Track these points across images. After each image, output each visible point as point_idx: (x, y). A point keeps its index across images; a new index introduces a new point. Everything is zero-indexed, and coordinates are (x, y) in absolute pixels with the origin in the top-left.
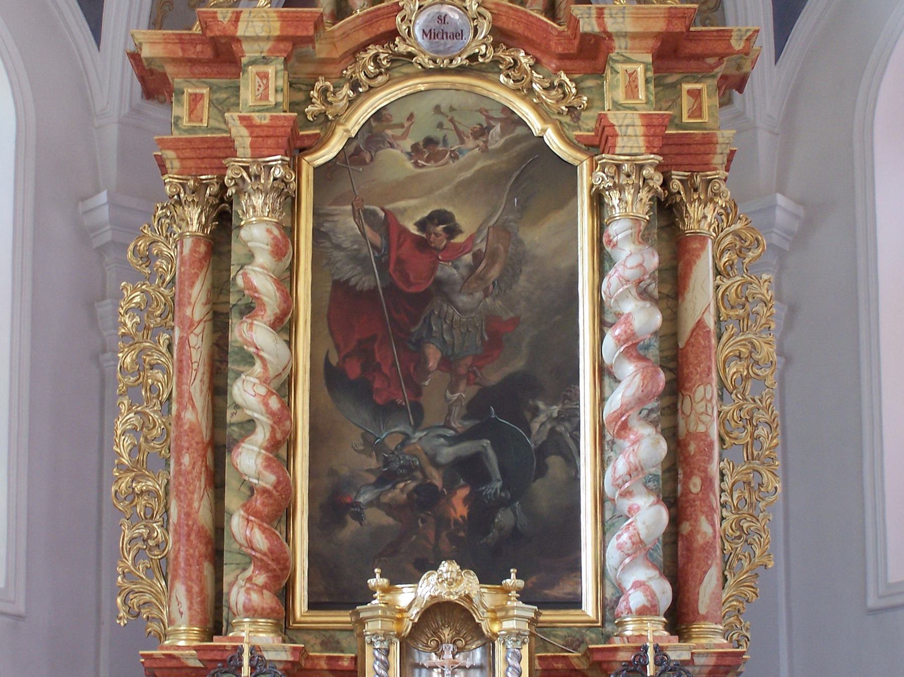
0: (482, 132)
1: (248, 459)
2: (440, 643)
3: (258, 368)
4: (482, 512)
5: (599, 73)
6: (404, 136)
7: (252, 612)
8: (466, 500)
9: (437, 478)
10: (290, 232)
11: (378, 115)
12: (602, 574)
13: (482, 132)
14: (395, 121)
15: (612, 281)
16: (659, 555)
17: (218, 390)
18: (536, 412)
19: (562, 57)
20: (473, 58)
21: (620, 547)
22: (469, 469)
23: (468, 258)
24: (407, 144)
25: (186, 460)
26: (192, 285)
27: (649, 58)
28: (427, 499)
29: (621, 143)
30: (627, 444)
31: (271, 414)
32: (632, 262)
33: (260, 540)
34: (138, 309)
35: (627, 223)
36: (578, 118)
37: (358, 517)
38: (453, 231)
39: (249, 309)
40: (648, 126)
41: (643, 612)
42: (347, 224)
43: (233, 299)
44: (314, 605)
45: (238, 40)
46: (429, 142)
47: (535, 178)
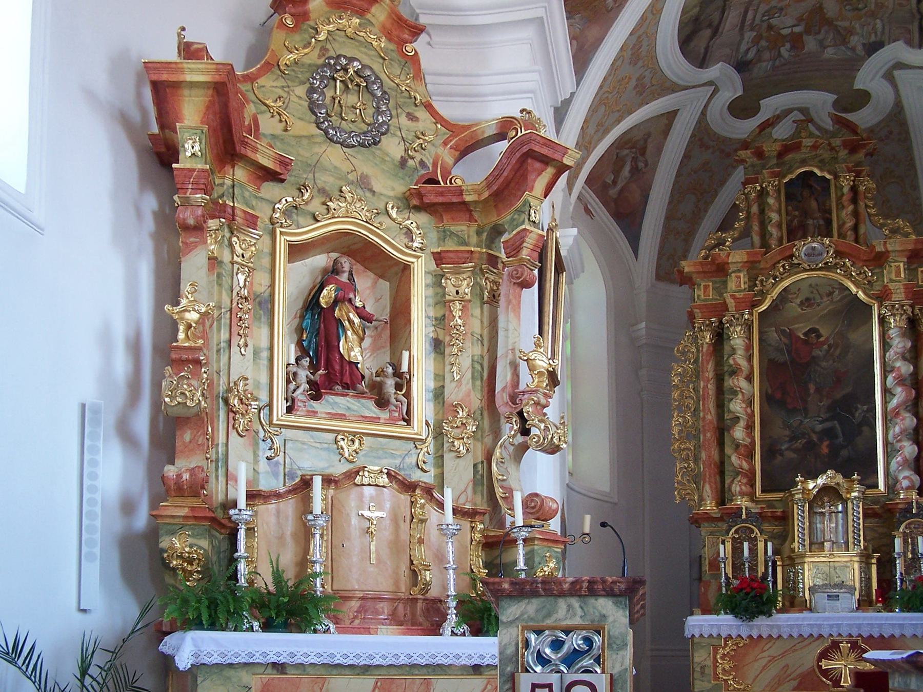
0: (830, 294)
1: (739, 433)
2: (823, 503)
3: (740, 396)
4: (835, 451)
5: (881, 266)
6: (796, 298)
7: (742, 494)
8: (828, 446)
9: (815, 438)
10: (750, 338)
11: (785, 290)
12: (887, 473)
13: (830, 294)
14: (792, 291)
15: (890, 354)
16: (912, 465)
17: (721, 406)
18: (857, 409)
19: (866, 261)
20: (826, 263)
21: (898, 463)
22: (829, 433)
23: (826, 347)
24: (798, 301)
25: (708, 435)
26: (708, 364)
27: (905, 260)
28: (811, 446)
29: (895, 297)
30: (898, 421)
31: (747, 414)
32: (900, 345)
33: (745, 465)
34: (680, 374)
35: (896, 330)
36: (872, 286)
37: (782, 455)
38: (819, 336)
39: (734, 372)
40: (906, 288)
41: (908, 488)
42: (773, 336)
43: (726, 369)
44: (763, 491)
45: (728, 263)
46: (807, 299)
47: (856, 313)
